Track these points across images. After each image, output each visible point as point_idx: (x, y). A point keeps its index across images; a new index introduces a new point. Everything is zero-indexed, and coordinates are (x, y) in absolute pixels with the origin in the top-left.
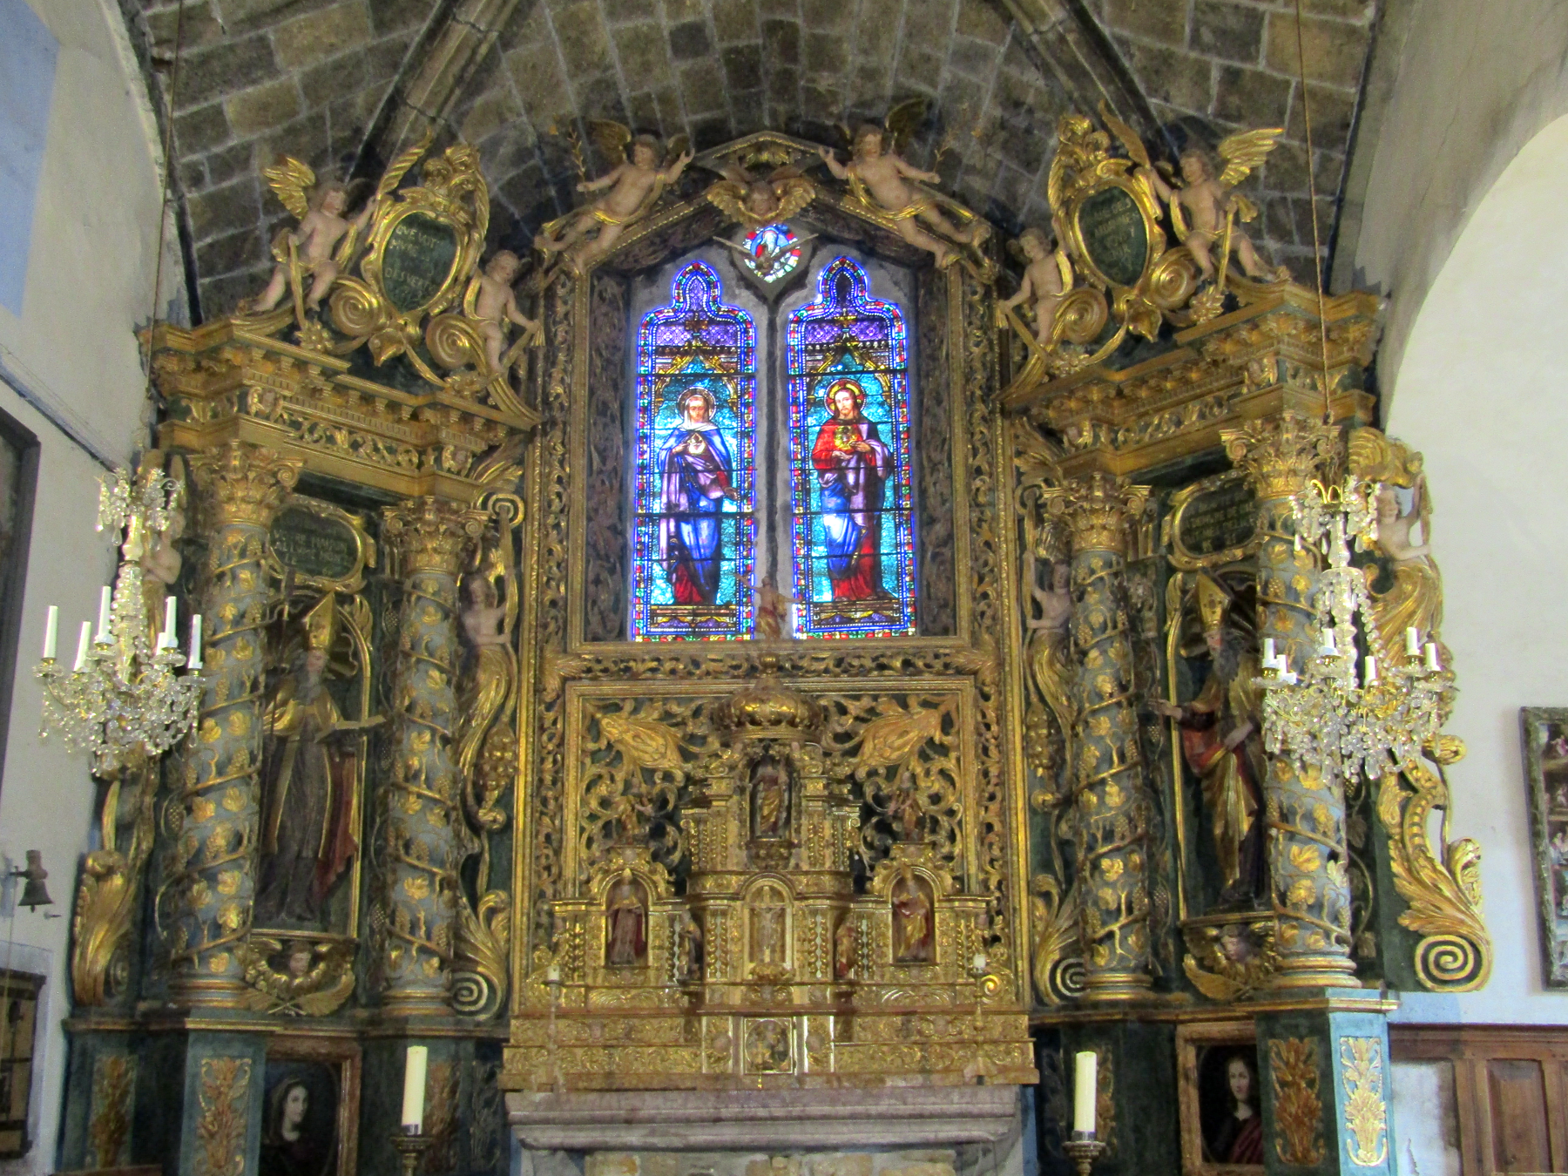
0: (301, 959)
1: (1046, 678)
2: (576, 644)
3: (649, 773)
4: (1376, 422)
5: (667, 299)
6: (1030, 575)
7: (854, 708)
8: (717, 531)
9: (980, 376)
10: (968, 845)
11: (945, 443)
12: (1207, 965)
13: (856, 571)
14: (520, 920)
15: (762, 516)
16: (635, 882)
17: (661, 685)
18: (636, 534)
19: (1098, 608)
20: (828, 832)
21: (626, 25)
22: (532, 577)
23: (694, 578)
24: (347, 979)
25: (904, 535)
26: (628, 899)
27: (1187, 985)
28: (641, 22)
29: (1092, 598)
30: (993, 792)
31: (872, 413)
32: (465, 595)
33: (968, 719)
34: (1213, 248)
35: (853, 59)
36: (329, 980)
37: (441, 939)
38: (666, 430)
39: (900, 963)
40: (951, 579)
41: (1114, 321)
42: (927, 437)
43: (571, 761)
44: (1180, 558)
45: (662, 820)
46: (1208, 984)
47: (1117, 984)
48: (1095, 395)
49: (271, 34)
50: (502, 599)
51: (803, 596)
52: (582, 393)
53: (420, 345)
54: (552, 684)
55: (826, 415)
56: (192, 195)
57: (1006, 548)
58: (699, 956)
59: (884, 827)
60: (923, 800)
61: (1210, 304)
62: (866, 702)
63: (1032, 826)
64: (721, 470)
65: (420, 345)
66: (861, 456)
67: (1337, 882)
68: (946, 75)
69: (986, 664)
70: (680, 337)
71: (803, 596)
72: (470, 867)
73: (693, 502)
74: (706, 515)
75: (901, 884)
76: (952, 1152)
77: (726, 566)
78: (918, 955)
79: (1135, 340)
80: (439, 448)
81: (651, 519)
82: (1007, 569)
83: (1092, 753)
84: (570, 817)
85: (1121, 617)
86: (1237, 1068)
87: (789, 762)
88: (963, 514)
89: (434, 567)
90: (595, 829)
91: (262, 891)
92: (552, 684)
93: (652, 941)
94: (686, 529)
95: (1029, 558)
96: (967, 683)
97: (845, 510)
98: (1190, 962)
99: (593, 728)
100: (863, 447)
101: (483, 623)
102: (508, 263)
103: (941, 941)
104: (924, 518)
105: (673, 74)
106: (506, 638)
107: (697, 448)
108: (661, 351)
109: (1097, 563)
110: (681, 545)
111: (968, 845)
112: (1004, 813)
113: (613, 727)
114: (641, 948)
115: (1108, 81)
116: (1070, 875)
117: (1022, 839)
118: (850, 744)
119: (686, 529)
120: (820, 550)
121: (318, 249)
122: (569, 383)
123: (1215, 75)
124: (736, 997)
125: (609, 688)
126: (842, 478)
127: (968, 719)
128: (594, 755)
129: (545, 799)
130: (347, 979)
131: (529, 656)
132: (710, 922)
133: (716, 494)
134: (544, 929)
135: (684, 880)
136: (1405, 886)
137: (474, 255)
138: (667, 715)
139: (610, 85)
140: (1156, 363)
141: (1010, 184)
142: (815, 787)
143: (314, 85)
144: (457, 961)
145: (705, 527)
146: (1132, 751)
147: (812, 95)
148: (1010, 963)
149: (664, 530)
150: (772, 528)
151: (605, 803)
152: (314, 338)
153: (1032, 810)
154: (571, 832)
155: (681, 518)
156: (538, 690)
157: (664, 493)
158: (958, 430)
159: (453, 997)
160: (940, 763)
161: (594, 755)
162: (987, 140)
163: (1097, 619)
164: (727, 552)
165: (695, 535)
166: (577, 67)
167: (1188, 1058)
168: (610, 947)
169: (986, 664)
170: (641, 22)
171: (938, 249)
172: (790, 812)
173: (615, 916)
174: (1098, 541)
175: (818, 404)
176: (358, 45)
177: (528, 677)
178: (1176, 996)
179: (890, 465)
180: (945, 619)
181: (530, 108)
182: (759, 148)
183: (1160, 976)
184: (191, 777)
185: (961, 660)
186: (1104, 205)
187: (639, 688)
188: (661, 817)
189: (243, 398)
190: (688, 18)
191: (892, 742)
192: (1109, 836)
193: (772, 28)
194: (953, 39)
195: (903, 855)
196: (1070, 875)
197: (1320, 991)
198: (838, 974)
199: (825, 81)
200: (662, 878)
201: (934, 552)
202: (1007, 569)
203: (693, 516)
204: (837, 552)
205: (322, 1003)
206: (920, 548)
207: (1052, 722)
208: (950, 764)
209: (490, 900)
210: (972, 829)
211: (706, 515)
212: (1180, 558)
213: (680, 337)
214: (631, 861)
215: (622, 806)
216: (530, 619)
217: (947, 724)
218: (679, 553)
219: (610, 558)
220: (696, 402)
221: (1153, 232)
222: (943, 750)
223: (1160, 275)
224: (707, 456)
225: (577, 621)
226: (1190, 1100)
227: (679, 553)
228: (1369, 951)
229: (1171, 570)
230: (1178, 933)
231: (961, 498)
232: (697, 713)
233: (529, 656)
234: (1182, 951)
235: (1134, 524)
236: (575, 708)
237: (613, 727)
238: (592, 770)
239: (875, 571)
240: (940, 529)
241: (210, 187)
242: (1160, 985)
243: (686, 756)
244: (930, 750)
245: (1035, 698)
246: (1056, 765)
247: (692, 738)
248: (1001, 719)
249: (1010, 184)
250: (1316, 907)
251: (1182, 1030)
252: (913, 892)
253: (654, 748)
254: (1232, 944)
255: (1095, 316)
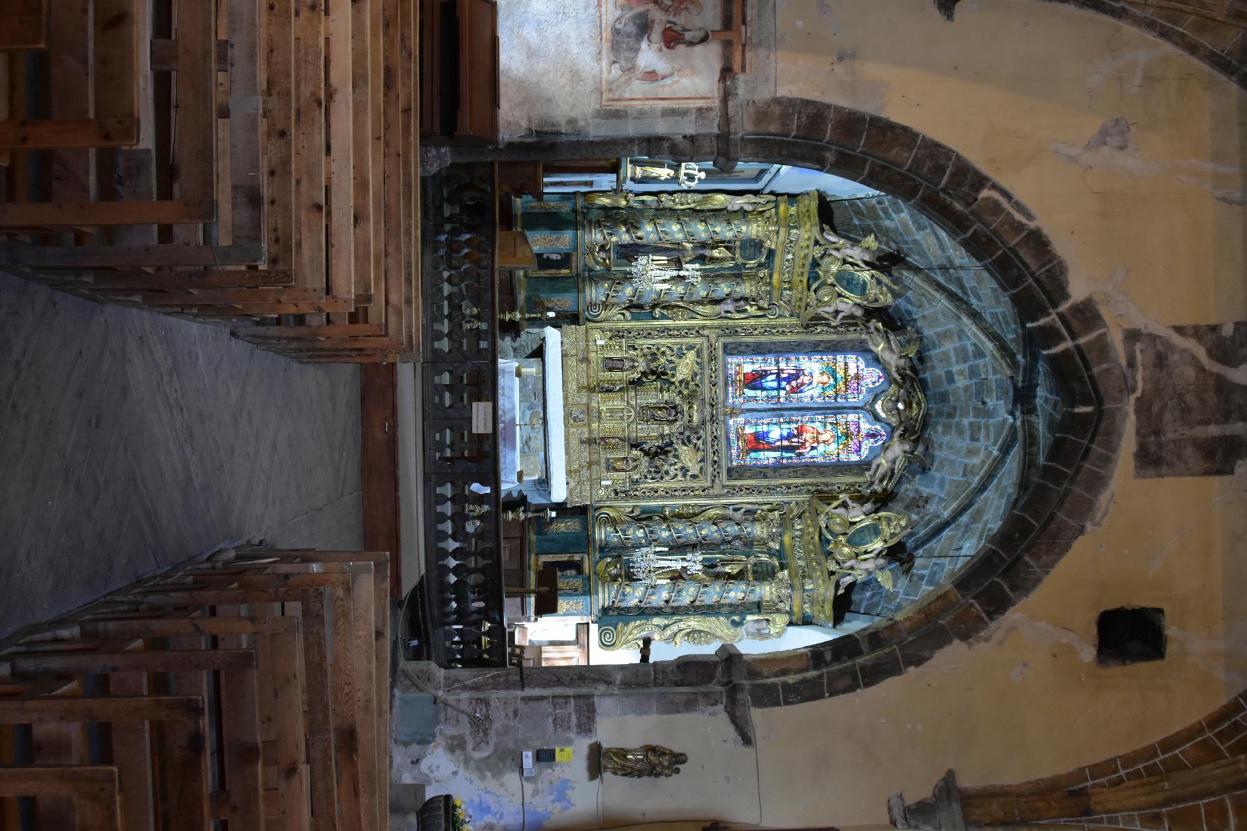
0: (603, 255)
1: (712, 512)
2: (722, 340)
3: (674, 369)
4: (791, 624)
5: (867, 366)
6: (749, 507)
7: (700, 442)
8: (773, 389)
9: (825, 489)
10: (651, 484)
11: (804, 476)
12: (608, 565)
13: (758, 443)
14: (620, 325)
15: (778, 406)
16: (633, 367)
17: (707, 372)
18: (771, 359)
19: (732, 529)
20: (650, 432)
21: (952, 354)
22: (744, 322)
23: (754, 381)
24: (598, 268)
25: (772, 461)
26: (627, 364)
27: (601, 558)
28: (953, 360)
29: (736, 528)
30: (669, 494)
31: (821, 448)
32: (737, 300)
33: (695, 484)
34: (852, 568)
35: (946, 439)
36: (597, 263)
37: (611, 300)
38: (813, 366)
39: (608, 460)
40: (750, 478)
41: (835, 535)
42: (810, 469)
43: (678, 340)
44: (752, 560)
45: (659, 374)
46: (601, 566)
47: (601, 534)
48: (811, 530)
49: (928, 231)
50: (738, 312)
51: (747, 422)
52: (819, 338)
53: (824, 284)
54: (706, 332)
55: (821, 430)
56: (874, 201)
57: (760, 499)
58: (608, 391)
59: (656, 454)
60: (666, 467)
61: (833, 566)
62: (702, 447)
63: (658, 507)
64: (797, 390)
65: (824, 284)
66: (803, 444)
67: (633, 602)
68: (938, 475)
69: (716, 491)
70: (852, 372)
71: (747, 422)
72: (641, 307)
73: (784, 379)
74: (779, 384)
75: (635, 460)
76: (490, 431)
77: (759, 392)
78: (611, 468)
79: (828, 541)
80: (790, 289)
81: (777, 363)
82: (752, 499)
83: (681, 527)
84: (659, 341)
85: (730, 538)
86: (574, 572)
87: (676, 420)
88: (773, 482)
89: (746, 289)
90: (654, 349)
91: (623, 246)
92: (706, 332)
93: (613, 374)
94: (774, 377)
95: (756, 507)
96: (709, 484)
97: (782, 438)
98: (609, 560)
99: (690, 348)
100: (807, 444)
101: (730, 306)
102: (859, 313)
103: (616, 475)
104: (777, 469)
105: (940, 371)
106: (723, 314)
107: (806, 379)
108: (846, 364)
109: (749, 530)
110: (766, 375)
111: (651, 484)
112: (662, 497)
113: (691, 356)
114: (611, 369)
115: (925, 534)
116: (638, 519)
117: (653, 503)
118: (687, 442)
119: (774, 377)
120: (765, 428)
121: (849, 252)
122: (821, 335)
123: (924, 572)
124: (594, 404)
125: (705, 353)
126: (795, 436)
127: (695, 484)
128: (680, 349)
129: (666, 332)
130: (598, 268)
131: (717, 322)
132: (619, 394)
133: (788, 388)
134: (618, 334)
135: (635, 384)
136: (632, 625)
137: (858, 301)
138: (696, 375)
139: (934, 348)
140: (818, 549)
141: (902, 500)
142: (667, 430)
143: (915, 241)
144: (606, 305)
145: (775, 384)
146: (681, 541)
147: (937, 423)
148: (608, 499)
149: (774, 369)
150: (774, 410)
151: (663, 353)
152: (818, 251)
153: (664, 507)
154: (652, 341)
155: (778, 374)
156: (704, 327)
157: (788, 368)
158: (807, 481)
159: (593, 305)
160: (680, 474)
161: (680, 349)
162: (917, 491)
163: (729, 529)
164: (765, 393)
165: (770, 382)
166: (938, 335)
167: (577, 557)
168: (611, 359)
169: (716, 491)
170: (953, 360)
171: (871, 473)
172: (659, 421)
173: (621, 360)
174: (758, 530)
175: (825, 426)
176: (932, 259)
177: (708, 323)
178: (598, 555)
179: (800, 455)
180: (735, 475)
181: (924, 317)
182: (919, 404)
183: (604, 549)
184: (660, 221)
185: (717, 481)
186: (875, 530)
187: (706, 364)
188: (660, 376)
189: (796, 228)
190: (956, 378)
191: (687, 456)
192: (651, 532)
193: (955, 408)
194: (948, 478)
195: (645, 461)
196: (638, 519)
197: (597, 593)
198: (602, 439)
199: (940, 428)
200: (636, 376)
201: (762, 471)
202: (752, 499)
203: (779, 379)
204: (764, 435)
205: (590, 262)
206: (766, 467)
207: (695, 515)
208: (679, 478)
209: (627, 314)
210: (656, 485)
211: (779, 384)
212: (752, 560)
213: (852, 372)
214: (642, 366)
215: (662, 360)
216: (730, 322)
217: (694, 476)
218: (763, 374)
219: (759, 350)
220: (825, 379)
221: (862, 549)
222: (684, 475)
223: (846, 550)
224: (803, 384)
225: (730, 340)
226: (564, 558)
227: (763, 374)
228: (611, 613)
229: (748, 557)
230: (619, 556)
231: (780, 482)
232: (697, 385)
233: (717, 322)
234: (613, 557)
235: (765, 544)
236: (698, 340)
237: (691, 356)
238: (675, 348)
239: (757, 450)
240: (770, 473)
241: (878, 207)
242: (602, 549)
243: (681, 382)
244: (685, 470)
245: (704, 509)
246: (680, 516)
247: (687, 383)
248: (695, 496)
249: (902, 500)
250: (624, 594)
251: (586, 556)
252: (632, 464)
253: (684, 369)
254: (614, 572)
255: (837, 529)
